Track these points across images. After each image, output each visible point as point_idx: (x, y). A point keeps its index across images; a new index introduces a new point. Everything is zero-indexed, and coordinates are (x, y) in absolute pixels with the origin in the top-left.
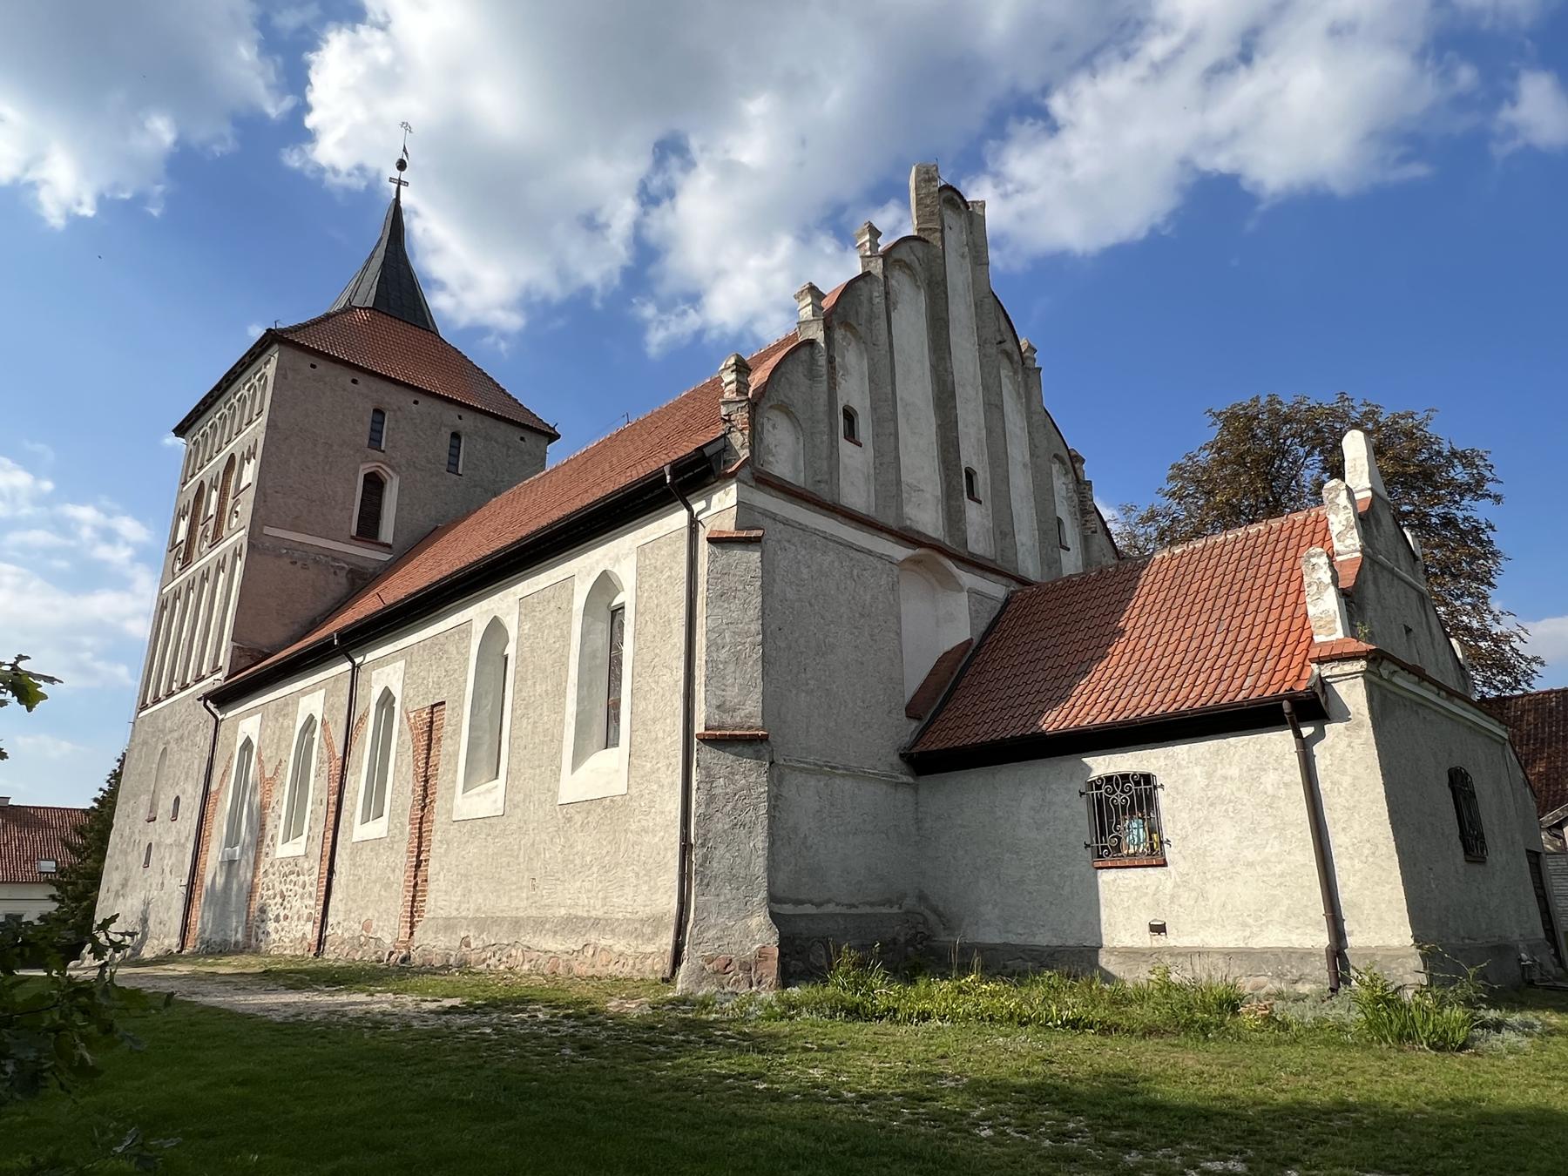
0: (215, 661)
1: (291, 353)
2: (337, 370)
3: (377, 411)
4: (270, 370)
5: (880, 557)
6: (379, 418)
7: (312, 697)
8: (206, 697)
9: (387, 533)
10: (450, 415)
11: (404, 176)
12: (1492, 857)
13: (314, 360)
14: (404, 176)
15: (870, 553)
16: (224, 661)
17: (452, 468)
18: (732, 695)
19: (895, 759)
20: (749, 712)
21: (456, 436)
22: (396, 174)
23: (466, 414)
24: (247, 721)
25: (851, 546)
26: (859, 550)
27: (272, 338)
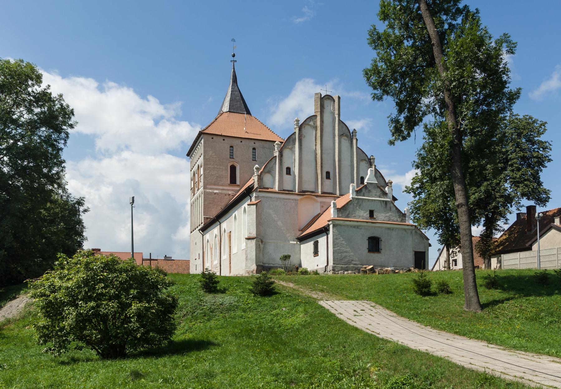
0: (200, 221)
1: (206, 136)
2: (219, 138)
3: (231, 147)
4: (202, 141)
5: (292, 200)
6: (232, 148)
7: (215, 230)
8: (199, 230)
9: (238, 182)
10: (251, 143)
11: (235, 59)
12: (289, 254)
13: (213, 136)
14: (235, 59)
15: (289, 199)
16: (203, 221)
17: (254, 159)
18: (251, 231)
19: (382, 251)
20: (254, 234)
21: (254, 149)
22: (232, 59)
23: (256, 142)
24: (207, 236)
25: (284, 199)
26: (286, 199)
27: (201, 134)
